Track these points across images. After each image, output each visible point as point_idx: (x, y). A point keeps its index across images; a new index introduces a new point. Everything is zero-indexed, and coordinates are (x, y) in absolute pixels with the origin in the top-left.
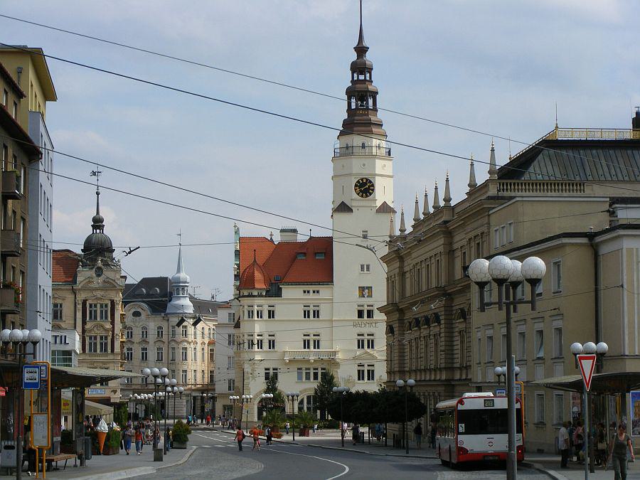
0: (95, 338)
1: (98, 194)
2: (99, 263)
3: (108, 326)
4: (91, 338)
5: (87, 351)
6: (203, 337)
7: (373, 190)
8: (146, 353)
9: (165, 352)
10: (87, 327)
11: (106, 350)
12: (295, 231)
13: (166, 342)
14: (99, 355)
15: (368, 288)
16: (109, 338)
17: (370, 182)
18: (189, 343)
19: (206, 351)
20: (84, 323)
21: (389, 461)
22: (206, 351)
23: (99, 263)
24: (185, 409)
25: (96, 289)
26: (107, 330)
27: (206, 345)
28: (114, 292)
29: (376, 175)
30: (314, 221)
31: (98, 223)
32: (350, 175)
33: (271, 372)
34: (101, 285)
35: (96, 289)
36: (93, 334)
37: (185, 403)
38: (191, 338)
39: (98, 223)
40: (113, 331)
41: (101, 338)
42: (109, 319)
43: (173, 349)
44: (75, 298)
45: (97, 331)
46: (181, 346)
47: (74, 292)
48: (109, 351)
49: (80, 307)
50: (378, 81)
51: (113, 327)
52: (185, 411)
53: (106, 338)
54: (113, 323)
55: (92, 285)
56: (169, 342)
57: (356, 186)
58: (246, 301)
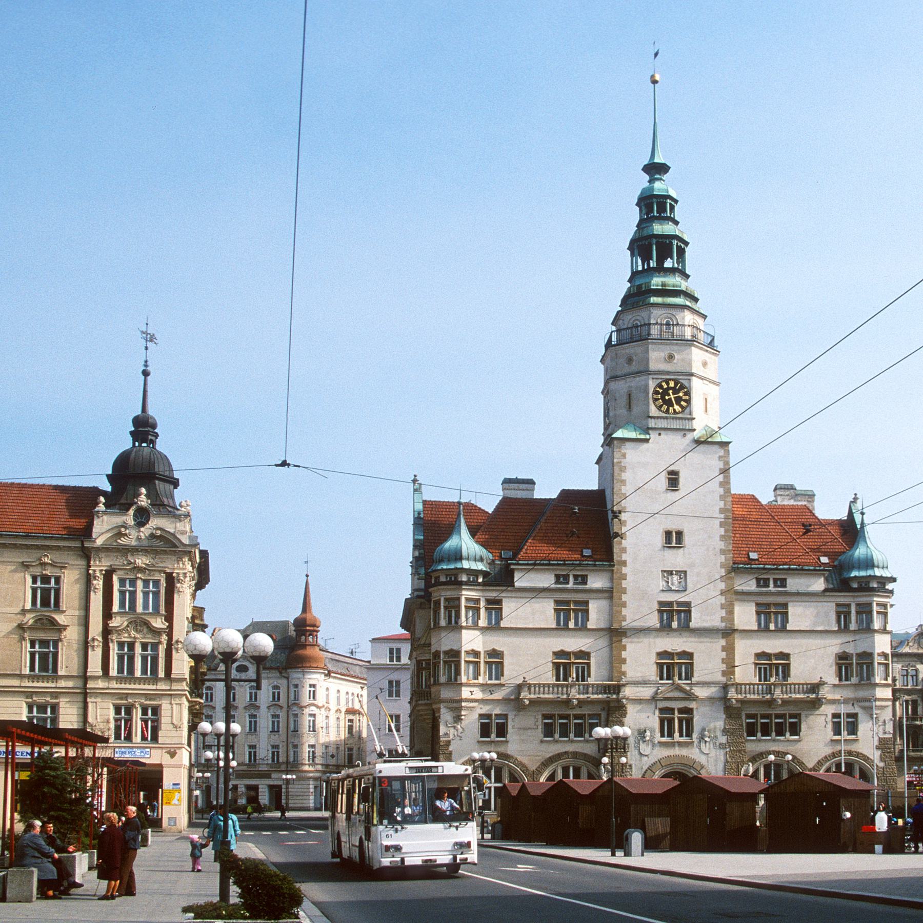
0: (131, 646)
1: (146, 374)
2: (143, 501)
3: (159, 623)
4: (121, 645)
5: (113, 672)
6: (339, 704)
7: (688, 402)
8: (255, 722)
9: (283, 719)
10: (115, 623)
11: (155, 670)
12: (531, 482)
13: (285, 709)
14: (139, 681)
15: (678, 572)
16: (162, 649)
17: (682, 387)
18: (318, 707)
19: (342, 724)
20: (107, 614)
21: (218, 784)
22: (342, 724)
23: (143, 501)
24: (312, 797)
25: (134, 550)
26: (156, 632)
27: (343, 713)
28: (174, 558)
29: (692, 375)
30: (563, 468)
31: (144, 429)
32: (646, 372)
33: (889, 586)
34: (145, 543)
35: (134, 550)
36: (125, 638)
37: (312, 790)
38: (320, 700)
39: (144, 429)
40: (170, 631)
41: (144, 646)
42: (162, 610)
43: (296, 715)
44: (89, 566)
45: (133, 633)
46: (307, 711)
47: (86, 554)
48: (161, 674)
49: (99, 584)
50: (687, 223)
51: (171, 627)
52: (312, 801)
53: (155, 646)
54: (169, 618)
55: (123, 541)
56: (288, 706)
57: (656, 392)
58: (443, 593)
